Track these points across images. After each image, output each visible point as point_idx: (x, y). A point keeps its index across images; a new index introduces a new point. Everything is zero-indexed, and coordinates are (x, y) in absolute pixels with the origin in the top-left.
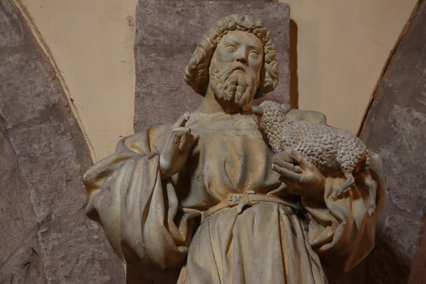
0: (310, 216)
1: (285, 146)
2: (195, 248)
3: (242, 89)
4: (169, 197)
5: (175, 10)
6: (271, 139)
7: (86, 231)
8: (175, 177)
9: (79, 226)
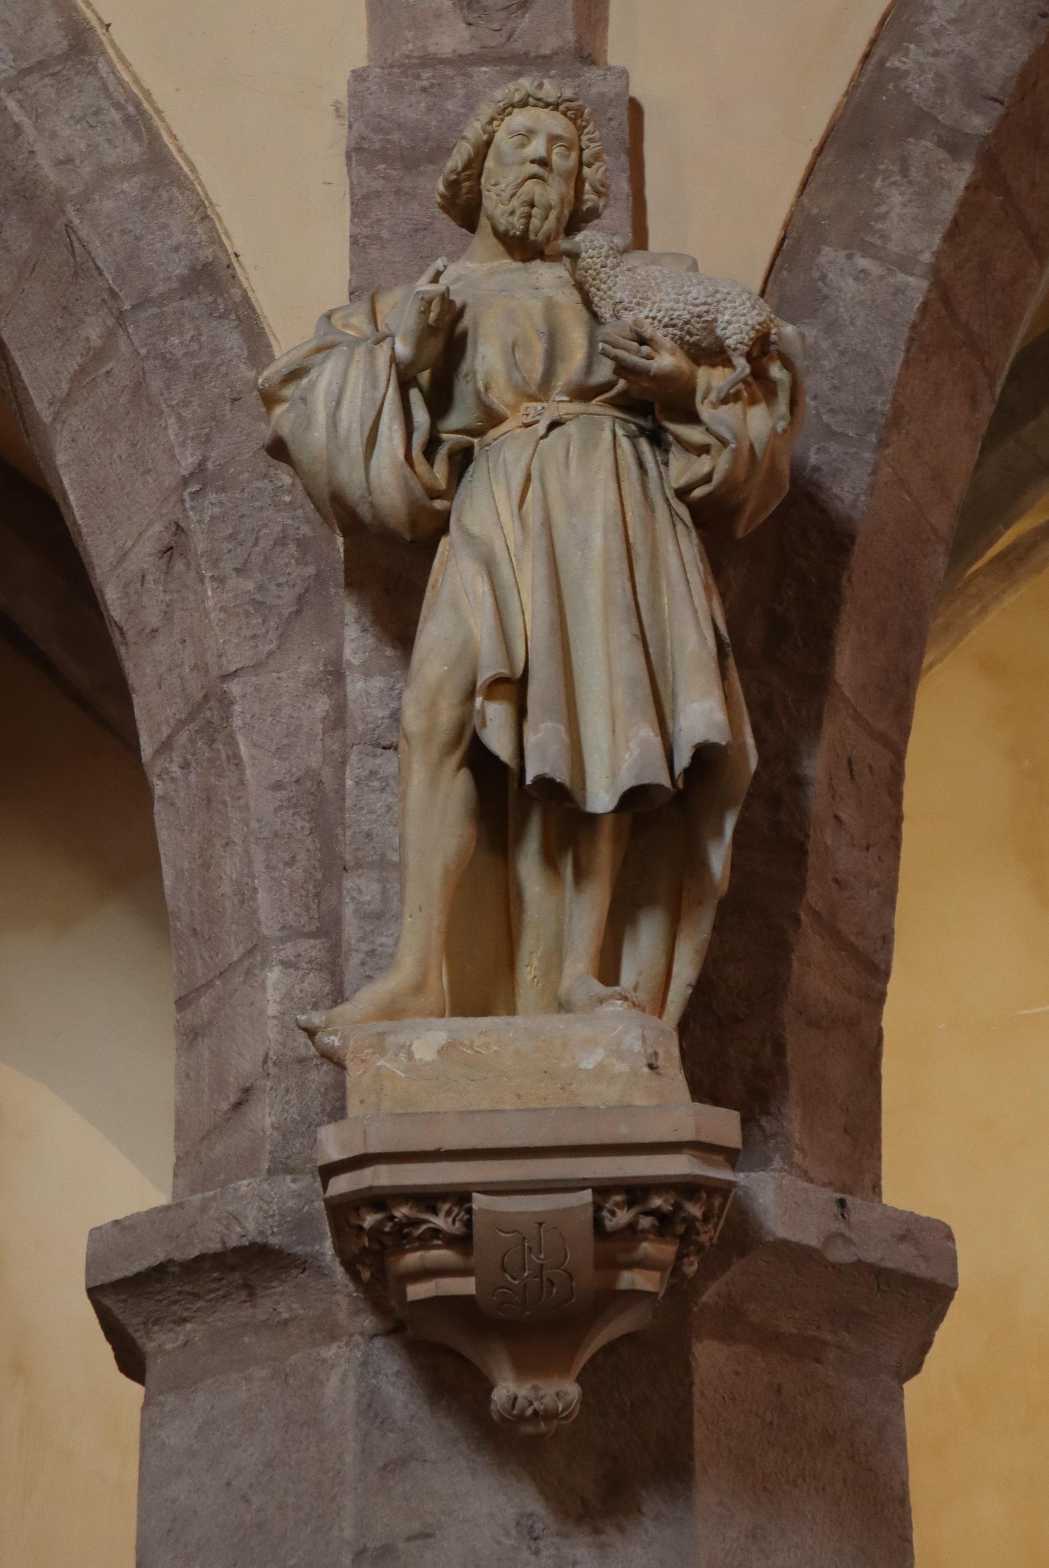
0: (671, 438)
2: (463, 502)
4: (414, 411)
5: (419, 84)
6: (596, 299)
7: (270, 487)
8: (425, 377)
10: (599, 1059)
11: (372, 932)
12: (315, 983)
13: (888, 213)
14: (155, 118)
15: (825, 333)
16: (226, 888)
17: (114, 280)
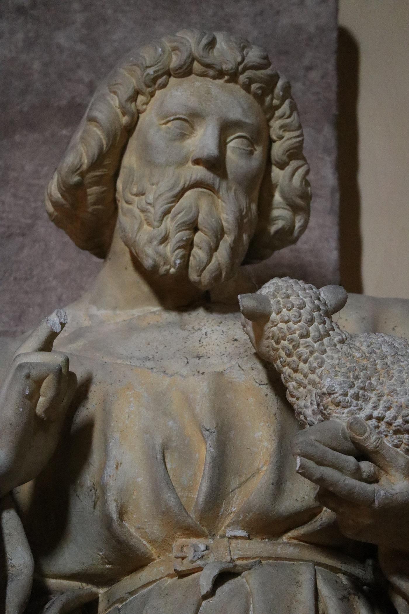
1: (332, 407)
3: (209, 244)
6: (292, 385)
8: (24, 491)
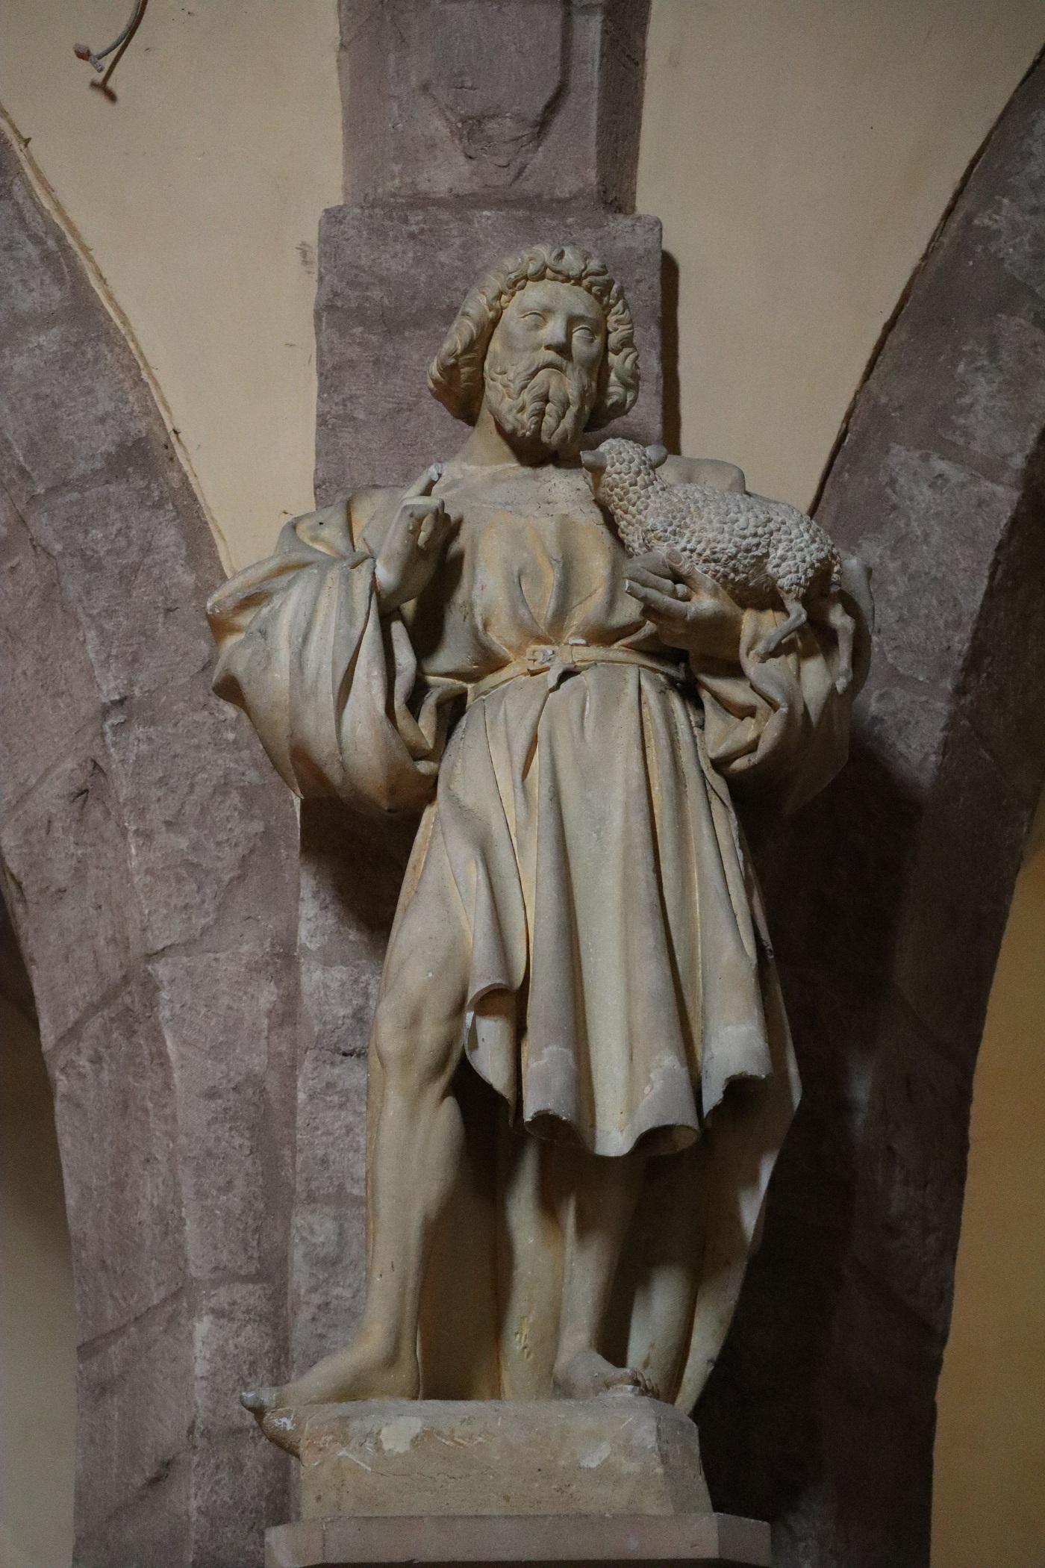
2: (454, 765)
5: (405, 229)
6: (622, 524)
7: (211, 721)
8: (409, 607)
9: (195, 711)
10: (605, 1456)
11: (326, 1281)
12: (252, 1337)
13: (972, 405)
14: (81, 255)
15: (892, 551)
16: (144, 1215)
17: (24, 456)
